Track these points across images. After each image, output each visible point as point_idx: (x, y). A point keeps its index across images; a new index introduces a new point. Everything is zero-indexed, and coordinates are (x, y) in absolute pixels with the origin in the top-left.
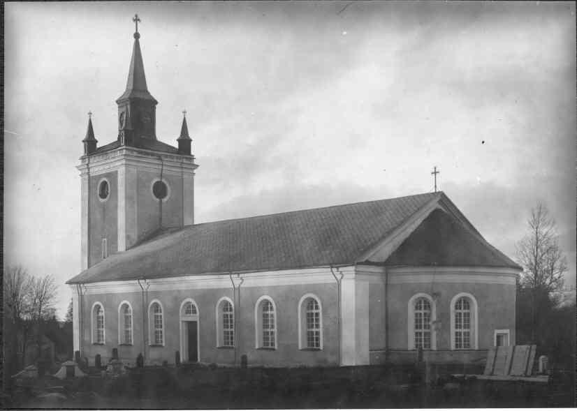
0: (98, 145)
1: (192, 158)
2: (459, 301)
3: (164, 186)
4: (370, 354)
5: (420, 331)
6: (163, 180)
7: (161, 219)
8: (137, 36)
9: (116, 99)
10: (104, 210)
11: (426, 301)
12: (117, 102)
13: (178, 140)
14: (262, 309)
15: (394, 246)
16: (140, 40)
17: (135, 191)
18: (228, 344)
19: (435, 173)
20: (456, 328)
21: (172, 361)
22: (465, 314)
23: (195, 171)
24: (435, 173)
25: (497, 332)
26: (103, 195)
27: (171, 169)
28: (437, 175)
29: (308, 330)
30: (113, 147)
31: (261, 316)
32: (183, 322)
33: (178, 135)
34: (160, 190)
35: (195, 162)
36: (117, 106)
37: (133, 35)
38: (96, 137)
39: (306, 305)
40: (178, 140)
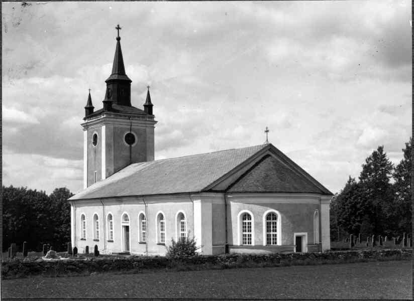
0: (95, 110)
1: (153, 117)
3: (133, 137)
4: (213, 248)
5: (273, 233)
6: (132, 133)
7: (131, 158)
8: (119, 39)
9: (105, 80)
10: (95, 152)
11: (249, 215)
12: (106, 82)
14: (242, 219)
16: (120, 41)
17: (112, 140)
19: (267, 131)
22: (248, 223)
23: (155, 125)
24: (267, 131)
25: (296, 234)
27: (138, 124)
28: (268, 133)
29: (276, 233)
30: (100, 113)
31: (242, 224)
32: (123, 226)
34: (130, 139)
35: (155, 119)
36: (106, 84)
38: (94, 105)
39: (242, 217)
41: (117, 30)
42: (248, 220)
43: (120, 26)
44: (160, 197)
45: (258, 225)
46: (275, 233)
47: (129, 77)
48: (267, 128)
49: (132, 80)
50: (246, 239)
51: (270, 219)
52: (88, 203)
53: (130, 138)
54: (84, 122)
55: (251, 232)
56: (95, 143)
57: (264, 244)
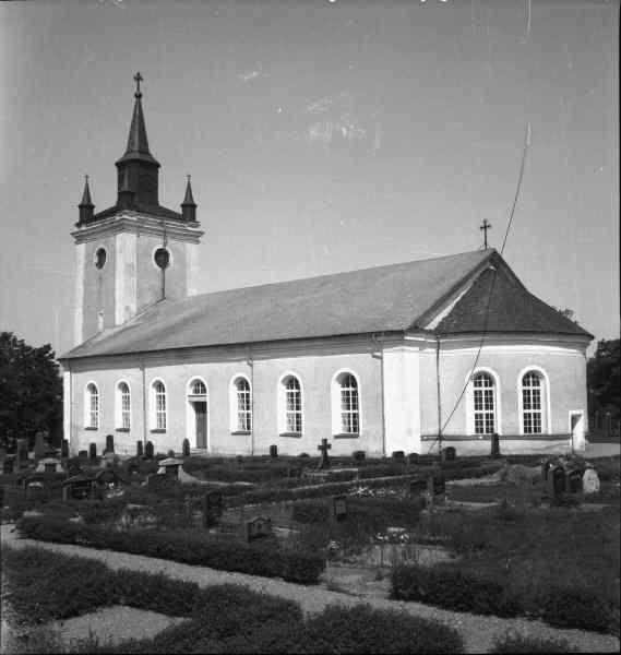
0: (96, 211)
2: (527, 376)
8: (139, 96)
9: (116, 160)
12: (117, 164)
13: (183, 206)
15: (141, 567)
16: (143, 100)
18: (530, 431)
19: (485, 227)
20: (525, 408)
21: (179, 449)
24: (485, 227)
26: (100, 264)
33: (182, 200)
37: (306, 452)
38: (93, 202)
40: (183, 206)
41: (135, 84)
42: (486, 386)
43: (142, 75)
44: (296, 344)
45: (506, 394)
46: (479, 412)
47: (154, 156)
48: (485, 222)
49: (160, 162)
50: (532, 425)
51: (529, 385)
52: (115, 362)
53: (162, 258)
54: (76, 229)
55: (525, 414)
56: (100, 264)
57: (522, 432)
